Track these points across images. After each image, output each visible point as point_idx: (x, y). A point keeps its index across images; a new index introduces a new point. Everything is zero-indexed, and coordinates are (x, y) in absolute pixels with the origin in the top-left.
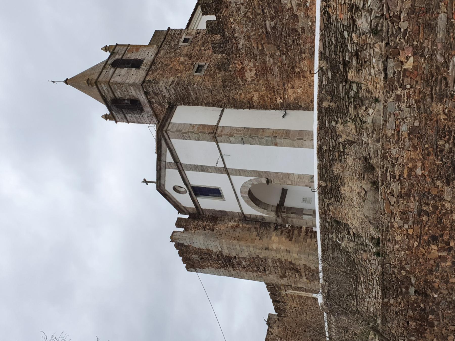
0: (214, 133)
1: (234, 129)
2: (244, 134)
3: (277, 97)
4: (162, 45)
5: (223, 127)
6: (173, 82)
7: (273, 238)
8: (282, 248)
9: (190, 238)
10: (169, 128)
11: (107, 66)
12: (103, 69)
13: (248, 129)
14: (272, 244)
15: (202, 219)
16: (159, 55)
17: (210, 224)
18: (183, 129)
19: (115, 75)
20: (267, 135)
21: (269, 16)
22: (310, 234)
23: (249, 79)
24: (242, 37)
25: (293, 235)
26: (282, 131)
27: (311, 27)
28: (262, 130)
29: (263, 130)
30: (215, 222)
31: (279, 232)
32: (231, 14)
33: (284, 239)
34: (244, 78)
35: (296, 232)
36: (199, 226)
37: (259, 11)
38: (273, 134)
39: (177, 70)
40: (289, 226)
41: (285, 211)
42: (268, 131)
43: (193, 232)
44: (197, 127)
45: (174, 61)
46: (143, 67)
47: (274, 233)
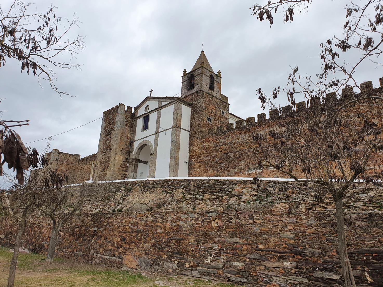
5: (180, 131)
7: (121, 157)
8: (116, 162)
10: (179, 104)
11: (211, 73)
16: (216, 99)
17: (129, 124)
31: (124, 160)
34: (205, 142)
35: (125, 169)
45: (213, 107)
47: (124, 158)
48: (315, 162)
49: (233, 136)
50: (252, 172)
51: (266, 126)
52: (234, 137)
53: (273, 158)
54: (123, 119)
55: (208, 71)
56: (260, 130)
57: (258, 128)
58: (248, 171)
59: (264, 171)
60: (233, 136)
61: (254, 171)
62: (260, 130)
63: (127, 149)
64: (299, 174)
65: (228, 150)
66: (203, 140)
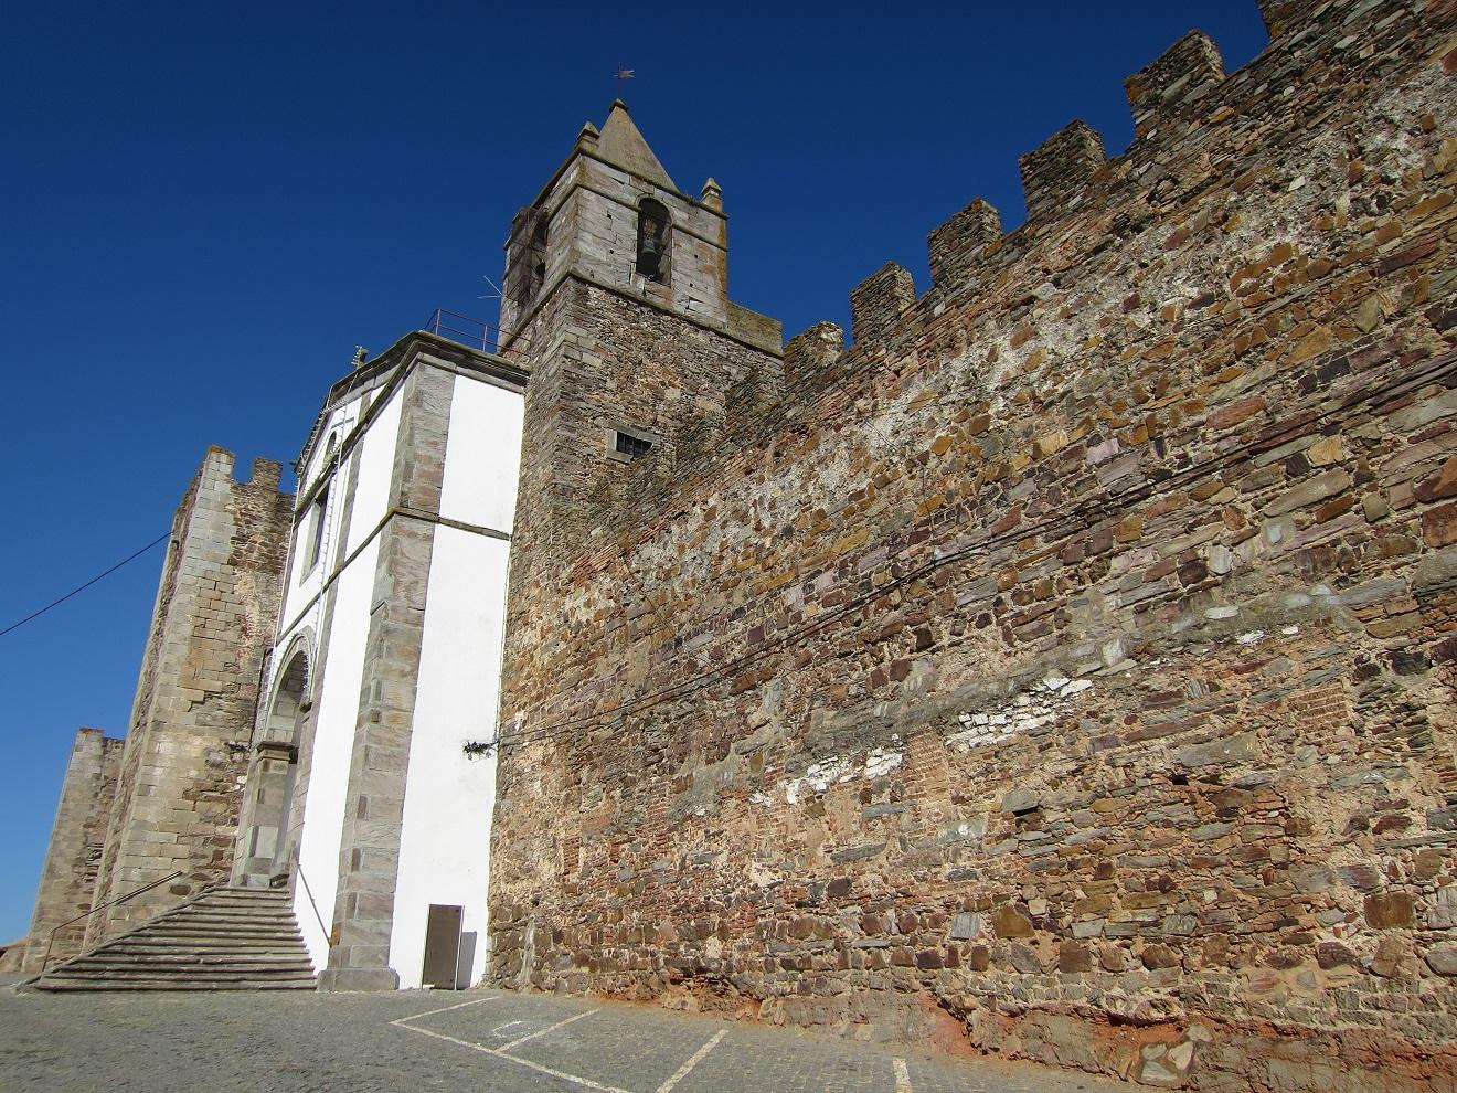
0: (403, 511)
1: (422, 574)
2: (394, 609)
3: (528, 708)
4: (728, 337)
5: (430, 539)
6: (582, 366)
7: (197, 741)
8: (158, 772)
9: (209, 501)
10: (430, 370)
11: (644, 186)
12: (631, 174)
13: (419, 622)
14: (175, 738)
15: (273, 531)
16: (686, 330)
17: (255, 555)
18: (426, 411)
19: (612, 205)
20: (387, 689)
21: (723, 639)
22: (210, 850)
23: (569, 604)
24: (672, 551)
25: (207, 799)
26: (402, 741)
27: (690, 817)
28: (408, 668)
29: (414, 674)
30: (262, 568)
31: (216, 757)
32: (731, 491)
33: (193, 773)
34: (572, 587)
35: (219, 808)
36: (248, 522)
37: (738, 600)
38: (391, 708)
39: (630, 378)
40: (242, 786)
41: (271, 771)
42: (404, 691)
43: (229, 507)
44: (432, 453)
45: (666, 372)
46: (642, 283)
47: (215, 743)
48: (670, 614)
49: (712, 502)
50: (829, 775)
51: (911, 361)
52: (714, 507)
53: (984, 621)
54: (219, 528)
55: (626, 178)
56: (875, 407)
57: (861, 394)
58: (797, 770)
59: (921, 759)
60: (712, 502)
61: (843, 770)
62: (875, 407)
63: (242, 694)
64: (1257, 766)
65: (685, 617)
66: (564, 576)
